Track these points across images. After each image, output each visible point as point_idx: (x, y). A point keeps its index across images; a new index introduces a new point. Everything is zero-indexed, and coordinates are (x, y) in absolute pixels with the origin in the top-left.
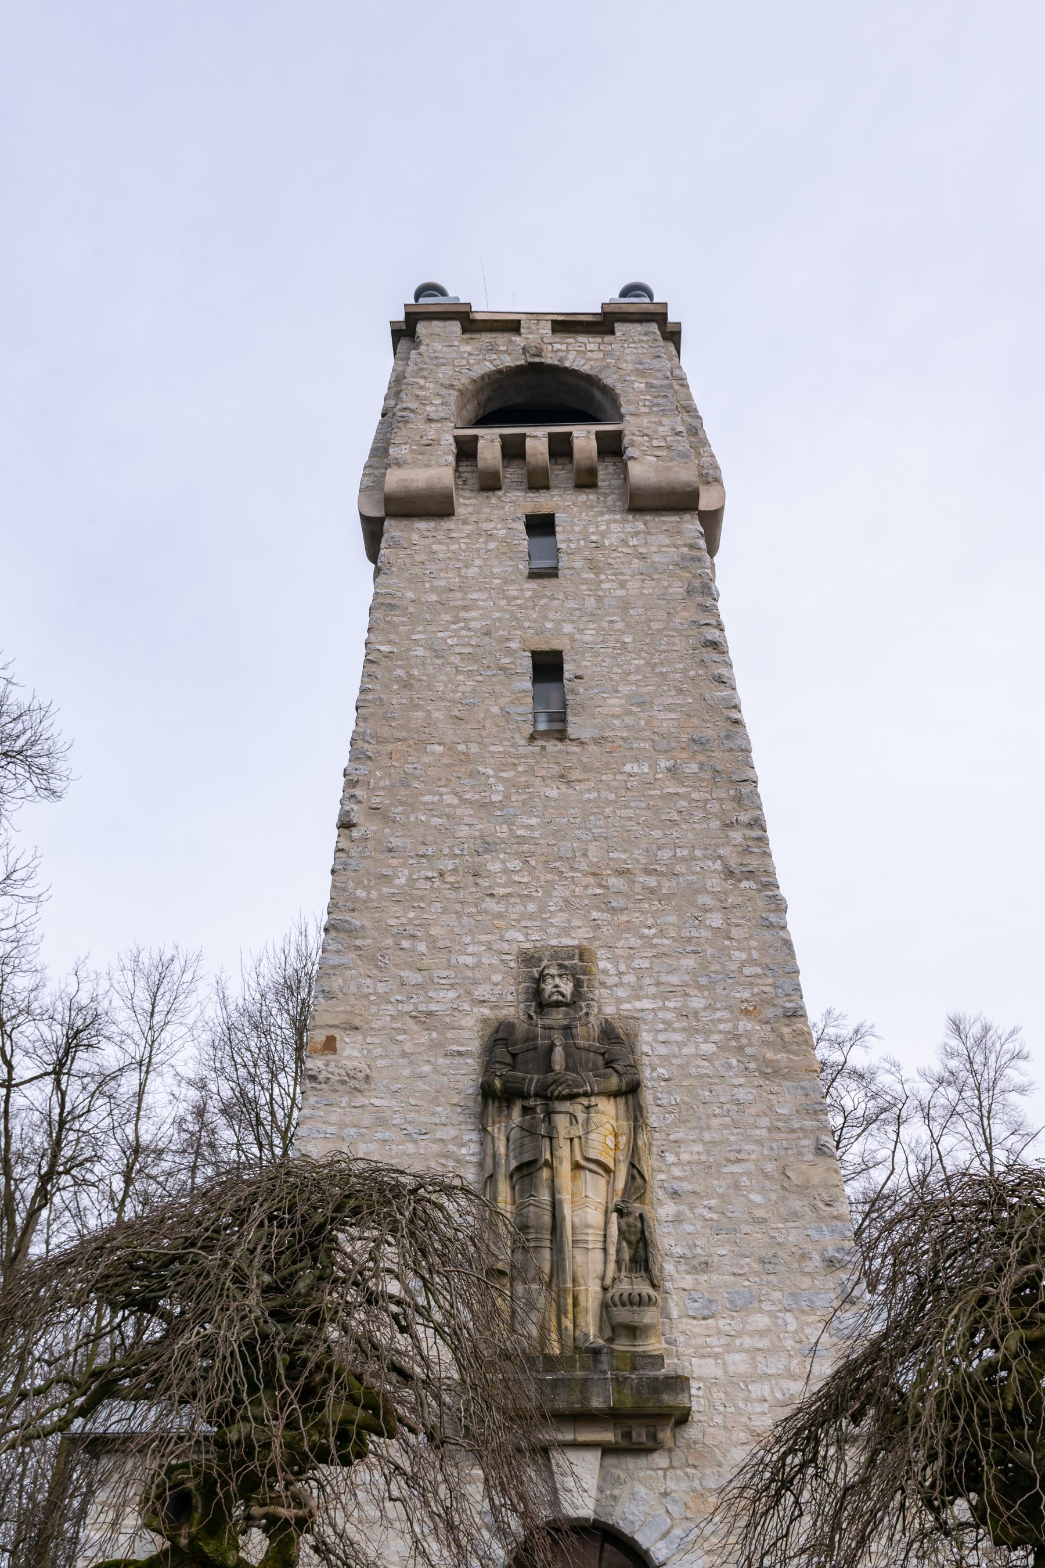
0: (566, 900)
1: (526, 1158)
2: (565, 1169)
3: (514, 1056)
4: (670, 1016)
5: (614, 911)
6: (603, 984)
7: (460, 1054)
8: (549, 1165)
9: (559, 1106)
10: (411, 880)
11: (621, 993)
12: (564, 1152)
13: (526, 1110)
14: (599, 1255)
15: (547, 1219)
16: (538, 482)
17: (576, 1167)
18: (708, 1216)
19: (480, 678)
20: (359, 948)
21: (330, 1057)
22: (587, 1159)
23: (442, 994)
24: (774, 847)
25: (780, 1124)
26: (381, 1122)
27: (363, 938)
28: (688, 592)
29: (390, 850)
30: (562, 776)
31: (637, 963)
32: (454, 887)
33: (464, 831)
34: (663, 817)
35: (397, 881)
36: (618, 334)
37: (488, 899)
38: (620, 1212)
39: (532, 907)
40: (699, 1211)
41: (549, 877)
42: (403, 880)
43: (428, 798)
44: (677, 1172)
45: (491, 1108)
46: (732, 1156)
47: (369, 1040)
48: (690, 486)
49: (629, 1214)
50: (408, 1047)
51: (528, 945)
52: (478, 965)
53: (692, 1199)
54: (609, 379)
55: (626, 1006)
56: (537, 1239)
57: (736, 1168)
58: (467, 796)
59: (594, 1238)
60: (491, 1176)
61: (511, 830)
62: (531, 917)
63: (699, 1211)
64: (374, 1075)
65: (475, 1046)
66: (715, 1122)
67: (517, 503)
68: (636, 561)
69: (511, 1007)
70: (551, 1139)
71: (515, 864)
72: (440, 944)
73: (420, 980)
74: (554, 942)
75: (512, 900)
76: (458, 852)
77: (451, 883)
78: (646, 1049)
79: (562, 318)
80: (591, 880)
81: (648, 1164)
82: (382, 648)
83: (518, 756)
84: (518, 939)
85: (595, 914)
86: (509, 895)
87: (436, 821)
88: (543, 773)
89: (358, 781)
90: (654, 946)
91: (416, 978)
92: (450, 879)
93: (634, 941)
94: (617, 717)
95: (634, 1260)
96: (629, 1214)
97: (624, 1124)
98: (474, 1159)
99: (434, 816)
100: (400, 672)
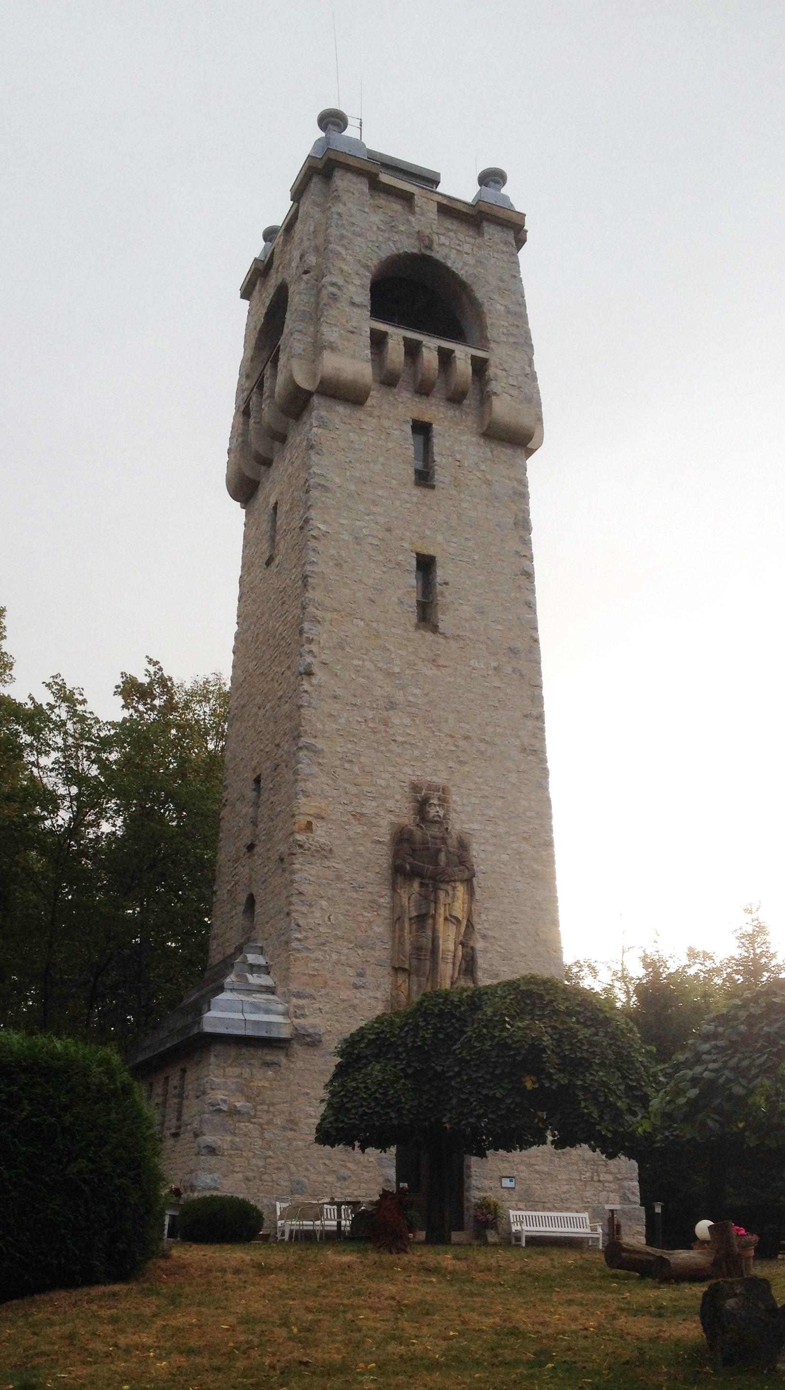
0: (436, 751)
1: (424, 912)
2: (441, 920)
3: (414, 851)
4: (488, 835)
5: (460, 762)
6: (455, 810)
7: (380, 842)
8: (434, 917)
9: (442, 886)
10: (348, 721)
11: (464, 818)
12: (442, 911)
13: (422, 885)
14: (451, 965)
15: (430, 946)
16: (423, 390)
17: (446, 919)
18: (500, 950)
19: (384, 569)
20: (320, 764)
21: (309, 834)
22: (451, 916)
23: (369, 803)
24: (548, 734)
25: (537, 906)
26: (339, 878)
27: (323, 758)
28: (515, 524)
29: (335, 697)
30: (434, 661)
31: (473, 799)
32: (374, 731)
33: (378, 692)
34: (491, 703)
35: (340, 721)
36: (486, 237)
37: (393, 743)
38: (462, 943)
39: (417, 753)
40: (495, 947)
41: (426, 733)
42: (343, 721)
43: (356, 662)
45: (400, 879)
46: (513, 920)
47: (329, 826)
48: (528, 430)
49: (467, 947)
50: (351, 833)
51: (414, 778)
52: (387, 787)
53: (492, 940)
54: (480, 294)
55: (466, 826)
56: (425, 955)
57: (514, 927)
58: (379, 665)
59: (450, 956)
60: (399, 919)
61: (404, 695)
62: (416, 759)
63: (495, 947)
64: (334, 849)
65: (387, 838)
66: (506, 900)
67: (405, 406)
68: (484, 486)
69: (407, 819)
70: (436, 903)
71: (407, 721)
72: (367, 769)
73: (357, 792)
74: (429, 779)
75: (406, 746)
76: (375, 706)
77: (372, 728)
78: (474, 853)
79: (445, 202)
80: (449, 740)
81: (475, 919)
82: (321, 526)
83: (409, 640)
84: (410, 773)
85: (451, 764)
86: (405, 742)
87: (361, 680)
88: (423, 656)
89: (313, 639)
90: (481, 790)
91: (353, 790)
92: (371, 725)
93: (471, 785)
94: (467, 621)
95: (466, 970)
96: (467, 947)
97: (466, 896)
98: (388, 906)
99: (359, 676)
100: (333, 551)
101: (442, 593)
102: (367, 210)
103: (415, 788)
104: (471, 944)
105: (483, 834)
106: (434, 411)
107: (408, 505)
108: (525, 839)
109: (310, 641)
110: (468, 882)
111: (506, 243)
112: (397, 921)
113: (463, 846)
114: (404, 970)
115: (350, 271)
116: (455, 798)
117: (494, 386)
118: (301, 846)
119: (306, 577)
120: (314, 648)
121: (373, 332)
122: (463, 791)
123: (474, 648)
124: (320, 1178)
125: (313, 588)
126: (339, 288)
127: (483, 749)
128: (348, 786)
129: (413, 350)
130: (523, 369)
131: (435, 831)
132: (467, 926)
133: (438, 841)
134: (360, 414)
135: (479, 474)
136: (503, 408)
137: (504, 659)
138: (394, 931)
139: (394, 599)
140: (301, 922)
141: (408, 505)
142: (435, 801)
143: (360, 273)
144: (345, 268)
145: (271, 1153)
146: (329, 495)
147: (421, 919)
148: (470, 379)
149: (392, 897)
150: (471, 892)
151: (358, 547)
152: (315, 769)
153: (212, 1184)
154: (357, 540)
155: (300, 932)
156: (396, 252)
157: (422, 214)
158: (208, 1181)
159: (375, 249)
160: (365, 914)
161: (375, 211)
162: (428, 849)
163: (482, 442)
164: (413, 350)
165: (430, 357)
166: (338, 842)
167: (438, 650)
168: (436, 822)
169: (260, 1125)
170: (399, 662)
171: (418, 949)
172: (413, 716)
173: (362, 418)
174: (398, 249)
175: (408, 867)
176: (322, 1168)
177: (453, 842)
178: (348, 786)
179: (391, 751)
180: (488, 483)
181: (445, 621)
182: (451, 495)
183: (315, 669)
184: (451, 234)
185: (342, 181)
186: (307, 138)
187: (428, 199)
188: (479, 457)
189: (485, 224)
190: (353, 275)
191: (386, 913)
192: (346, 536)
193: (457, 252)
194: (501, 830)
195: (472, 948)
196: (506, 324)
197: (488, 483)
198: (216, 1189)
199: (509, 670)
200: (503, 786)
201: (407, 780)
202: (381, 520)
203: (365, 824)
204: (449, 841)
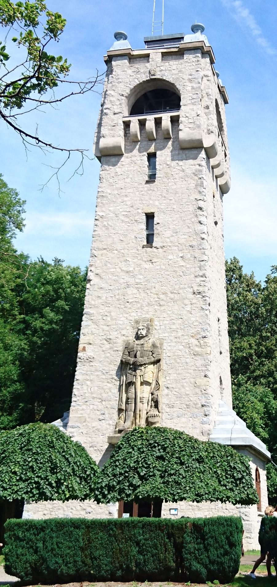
2: (138, 384)
15: (134, 396)
30: (151, 261)
44: (169, 382)
51: (137, 317)
52: (124, 324)
66: (180, 368)
71: (135, 291)
74: (144, 316)
80: (156, 296)
84: (135, 316)
90: (170, 317)
92: (117, 297)
107: (142, 193)
117: (181, 126)
128: (104, 327)
135: (178, 168)
146: (105, 199)
151: (117, 218)
152: (90, 322)
156: (138, 83)
165: (150, 125)
170: (133, 266)
181: (157, 241)
192: (112, 215)
194: (180, 334)
196: (191, 95)
199: (189, 256)
201: (133, 320)
202: (129, 203)
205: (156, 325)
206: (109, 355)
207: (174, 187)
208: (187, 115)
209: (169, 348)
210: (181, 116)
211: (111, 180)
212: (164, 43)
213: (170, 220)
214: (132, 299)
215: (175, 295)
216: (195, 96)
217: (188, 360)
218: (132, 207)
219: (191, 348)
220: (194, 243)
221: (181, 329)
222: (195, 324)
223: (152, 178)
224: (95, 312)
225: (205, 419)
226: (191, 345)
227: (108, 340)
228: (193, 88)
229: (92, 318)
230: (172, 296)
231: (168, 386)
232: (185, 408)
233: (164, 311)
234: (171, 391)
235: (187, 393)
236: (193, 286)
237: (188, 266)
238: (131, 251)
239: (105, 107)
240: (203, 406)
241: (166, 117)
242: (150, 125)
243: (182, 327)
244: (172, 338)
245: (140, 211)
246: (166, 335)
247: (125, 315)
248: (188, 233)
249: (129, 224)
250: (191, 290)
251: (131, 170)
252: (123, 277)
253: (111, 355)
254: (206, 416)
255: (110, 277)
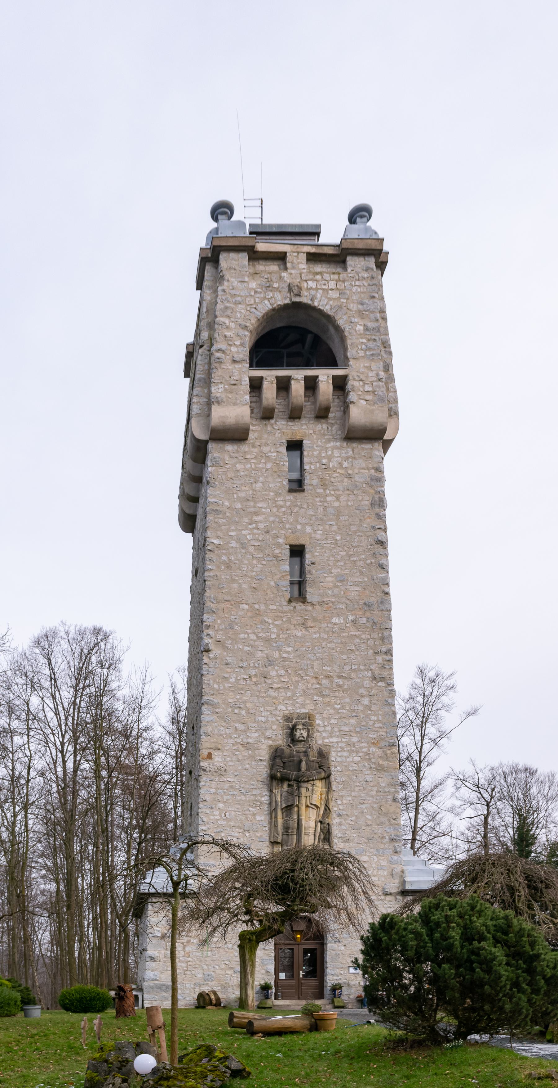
0: (304, 691)
1: (289, 804)
2: (303, 808)
4: (343, 745)
7: (261, 760)
8: (298, 806)
11: (325, 735)
12: (304, 802)
13: (289, 786)
14: (312, 837)
15: (296, 825)
16: (295, 414)
17: (307, 806)
19: (264, 563)
20: (217, 713)
23: (253, 734)
26: (231, 787)
28: (372, 504)
29: (227, 664)
30: (303, 624)
34: (348, 648)
35: (231, 680)
38: (321, 822)
39: (289, 694)
44: (341, 807)
45: (275, 783)
46: (362, 802)
50: (240, 757)
51: (287, 712)
52: (267, 721)
53: (346, 817)
59: (311, 831)
62: (289, 699)
64: (227, 769)
65: (266, 757)
66: (357, 789)
67: (283, 429)
68: (346, 480)
71: (282, 672)
72: (251, 711)
74: (298, 711)
78: (333, 759)
80: (314, 681)
81: (332, 804)
83: (283, 612)
84: (284, 709)
85: (316, 698)
87: (247, 648)
88: (294, 622)
90: (339, 713)
91: (241, 727)
92: (254, 679)
93: (332, 711)
95: (324, 839)
97: (324, 790)
100: (224, 558)
101: (310, 572)
102: (246, 279)
103: (287, 719)
104: (327, 821)
105: (340, 744)
106: (306, 429)
107: (283, 509)
108: (374, 743)
109: (208, 627)
110: (327, 778)
111: (367, 269)
112: (273, 812)
113: (322, 755)
114: (278, 843)
115: (232, 335)
116: (318, 722)
117: (352, 396)
118: (204, 770)
119: (205, 581)
120: (211, 632)
121: (251, 379)
122: (325, 716)
123: (336, 608)
124: (223, 972)
125: (210, 588)
126: (223, 352)
127: (341, 683)
128: (237, 725)
129: (284, 386)
130: (378, 375)
131: (300, 747)
132: (325, 810)
133: (301, 754)
134: (244, 447)
135: (341, 471)
136: (359, 413)
137: (360, 613)
138: (271, 818)
139: (272, 583)
140: (205, 819)
141: (283, 509)
142: (300, 727)
143: (240, 334)
144: (228, 334)
145: (190, 959)
146: (220, 516)
147: (288, 809)
148: (331, 397)
149: (270, 796)
150: (329, 787)
151: (244, 551)
152: (214, 717)
153: (154, 977)
154: (243, 546)
155: (205, 825)
156: (270, 307)
157: (293, 268)
158: (152, 976)
159: (253, 310)
160: (251, 809)
161: (253, 279)
162: (293, 761)
163: (345, 444)
164: (284, 386)
165: (298, 388)
166: (230, 764)
167: (306, 615)
168: (301, 741)
169: (183, 943)
170: (275, 630)
171: (287, 828)
172: (286, 669)
173: (246, 450)
174: (272, 305)
175: (279, 775)
176: (223, 966)
177: (313, 755)
178: (237, 725)
179: (269, 696)
180: (350, 477)
181: (312, 593)
182: (318, 493)
183: (211, 647)
184: (318, 277)
185: (226, 260)
186: (200, 231)
187: (298, 253)
188: (342, 458)
189: (349, 258)
190: (235, 338)
191: (266, 807)
192: (234, 544)
193: (323, 291)
194: (355, 739)
195: (328, 824)
196: (364, 341)
197: (350, 477)
198: (157, 980)
199: (364, 620)
200: (357, 708)
201: (282, 715)
202: (261, 525)
203: (250, 749)
204: (310, 753)
205: (319, 725)
206: (247, 766)
207: (336, 504)
208: (361, 377)
209: (339, 759)
210: (350, 377)
211: (229, 484)
212: (271, 238)
213: (331, 559)
214: (277, 683)
215: (346, 681)
216: (371, 344)
217: (368, 778)
218: (267, 532)
219: (373, 760)
220: (373, 600)
221: (356, 732)
222: (376, 725)
223: (298, 485)
224: (220, 702)
225: (395, 858)
226: (371, 756)
227: (247, 745)
228: (366, 328)
229: (217, 710)
230: (340, 682)
231: (341, 812)
232: (366, 843)
233: (329, 704)
234: (345, 820)
235: (369, 822)
236: (372, 667)
237: (363, 636)
238: (271, 607)
239: (215, 347)
240: (392, 840)
241: (325, 376)
242: (298, 388)
243: (358, 729)
244: (343, 745)
245: (281, 541)
246: (334, 740)
247: (269, 708)
248: (361, 582)
249: (264, 563)
250: (369, 674)
251: (261, 469)
252: (260, 648)
253: (251, 767)
254: (397, 853)
255: (241, 647)
